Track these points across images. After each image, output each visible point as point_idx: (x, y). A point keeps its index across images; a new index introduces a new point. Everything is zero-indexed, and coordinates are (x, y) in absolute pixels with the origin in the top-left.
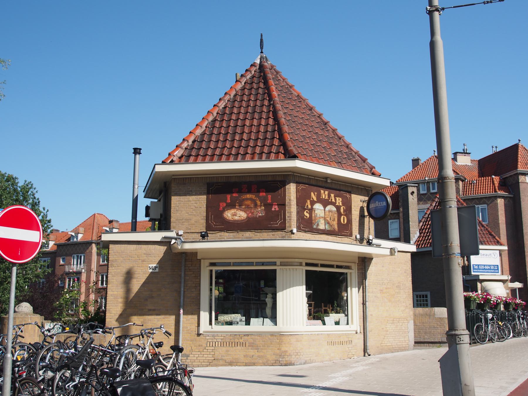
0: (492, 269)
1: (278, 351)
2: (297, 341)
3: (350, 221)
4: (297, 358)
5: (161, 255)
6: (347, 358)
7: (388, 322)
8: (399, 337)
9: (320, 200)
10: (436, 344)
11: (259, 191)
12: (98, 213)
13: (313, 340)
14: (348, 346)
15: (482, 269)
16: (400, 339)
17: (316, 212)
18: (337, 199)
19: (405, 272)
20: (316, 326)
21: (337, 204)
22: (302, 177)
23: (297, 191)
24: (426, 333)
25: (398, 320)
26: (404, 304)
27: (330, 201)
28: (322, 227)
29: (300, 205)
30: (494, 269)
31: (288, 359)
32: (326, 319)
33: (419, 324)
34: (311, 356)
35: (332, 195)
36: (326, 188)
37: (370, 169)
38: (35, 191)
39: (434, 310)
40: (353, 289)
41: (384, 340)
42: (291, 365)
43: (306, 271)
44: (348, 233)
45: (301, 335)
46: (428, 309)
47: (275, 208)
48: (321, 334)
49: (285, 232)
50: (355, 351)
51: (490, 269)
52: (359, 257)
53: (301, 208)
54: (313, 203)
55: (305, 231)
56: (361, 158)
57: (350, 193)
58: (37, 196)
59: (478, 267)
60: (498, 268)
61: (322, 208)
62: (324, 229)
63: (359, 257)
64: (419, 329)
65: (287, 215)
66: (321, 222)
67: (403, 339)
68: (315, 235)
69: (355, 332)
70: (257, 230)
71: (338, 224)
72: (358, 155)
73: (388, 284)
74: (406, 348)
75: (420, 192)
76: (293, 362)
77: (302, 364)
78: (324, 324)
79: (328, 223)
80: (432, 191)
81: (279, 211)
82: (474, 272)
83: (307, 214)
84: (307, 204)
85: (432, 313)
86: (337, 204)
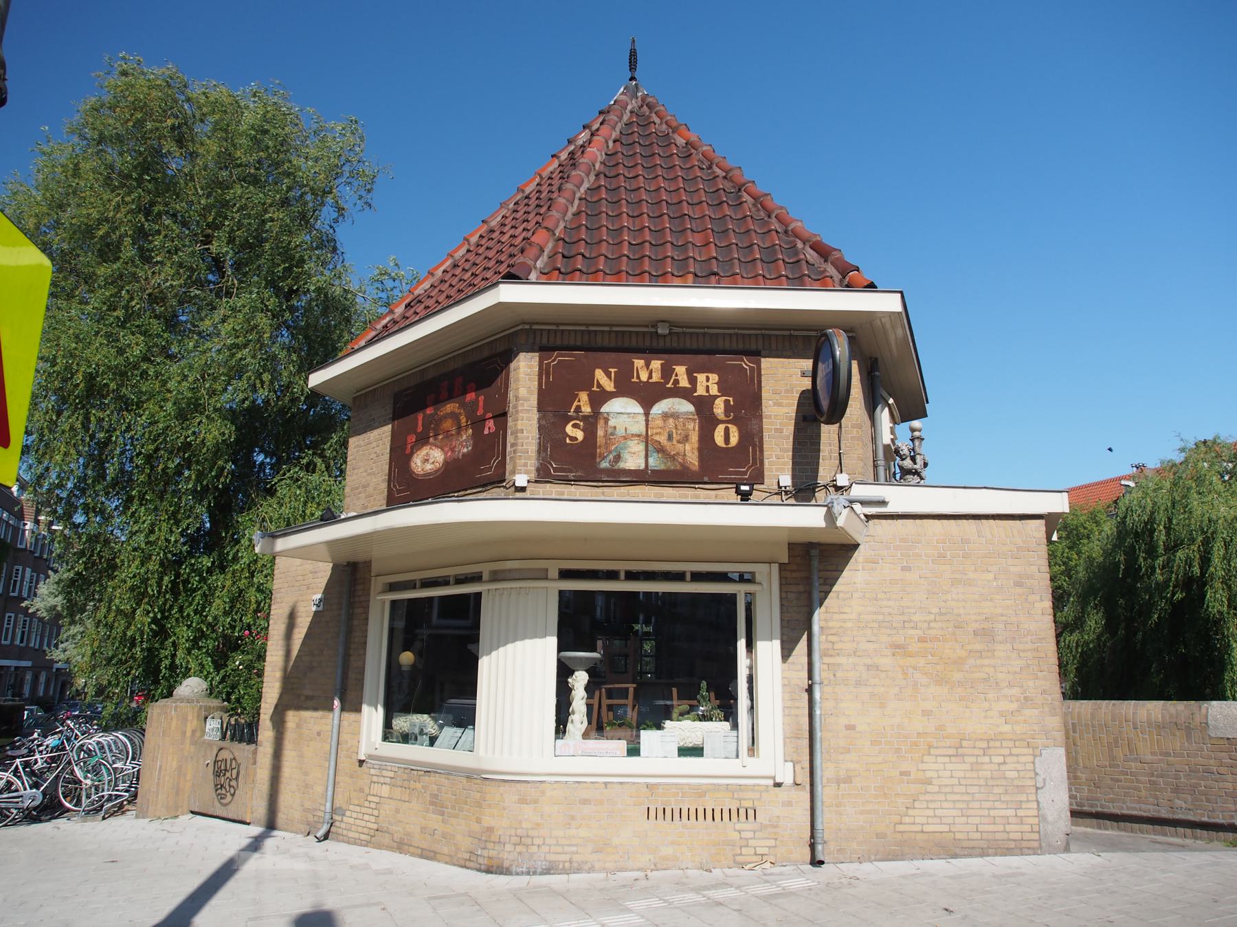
1: (476, 827)
2: (523, 801)
3: (752, 441)
4: (520, 853)
5: (329, 573)
6: (731, 863)
7: (933, 751)
8: (988, 804)
9: (626, 387)
10: (1221, 834)
11: (465, 393)
13: (585, 802)
14: (738, 826)
16: (992, 813)
17: (611, 423)
18: (701, 377)
19: (1018, 584)
21: (701, 391)
22: (563, 331)
23: (543, 371)
24: (1177, 790)
25: (984, 745)
26: (1015, 691)
27: (669, 385)
28: (633, 459)
29: (550, 409)
31: (493, 853)
32: (648, 737)
33: (1149, 758)
34: (574, 849)
35: (681, 370)
36: (649, 352)
37: (840, 277)
39: (1203, 711)
41: (911, 812)
42: (501, 873)
43: (561, 592)
44: (745, 473)
45: (538, 784)
46: (1186, 706)
48: (621, 783)
49: (504, 487)
50: (772, 843)
52: (791, 546)
53: (555, 416)
54: (600, 398)
55: (567, 481)
56: (817, 253)
57: (756, 354)
61: (640, 410)
62: (642, 467)
63: (791, 546)
64: (1153, 775)
65: (510, 439)
66: (629, 450)
67: (1011, 812)
68: (605, 489)
69: (771, 782)
70: (459, 491)
71: (700, 450)
72: (811, 247)
73: (932, 625)
74: (1024, 844)
76: (506, 864)
77: (535, 873)
78: (634, 751)
79: (661, 450)
81: (495, 435)
84: (576, 403)
85: (1198, 718)
86: (701, 391)
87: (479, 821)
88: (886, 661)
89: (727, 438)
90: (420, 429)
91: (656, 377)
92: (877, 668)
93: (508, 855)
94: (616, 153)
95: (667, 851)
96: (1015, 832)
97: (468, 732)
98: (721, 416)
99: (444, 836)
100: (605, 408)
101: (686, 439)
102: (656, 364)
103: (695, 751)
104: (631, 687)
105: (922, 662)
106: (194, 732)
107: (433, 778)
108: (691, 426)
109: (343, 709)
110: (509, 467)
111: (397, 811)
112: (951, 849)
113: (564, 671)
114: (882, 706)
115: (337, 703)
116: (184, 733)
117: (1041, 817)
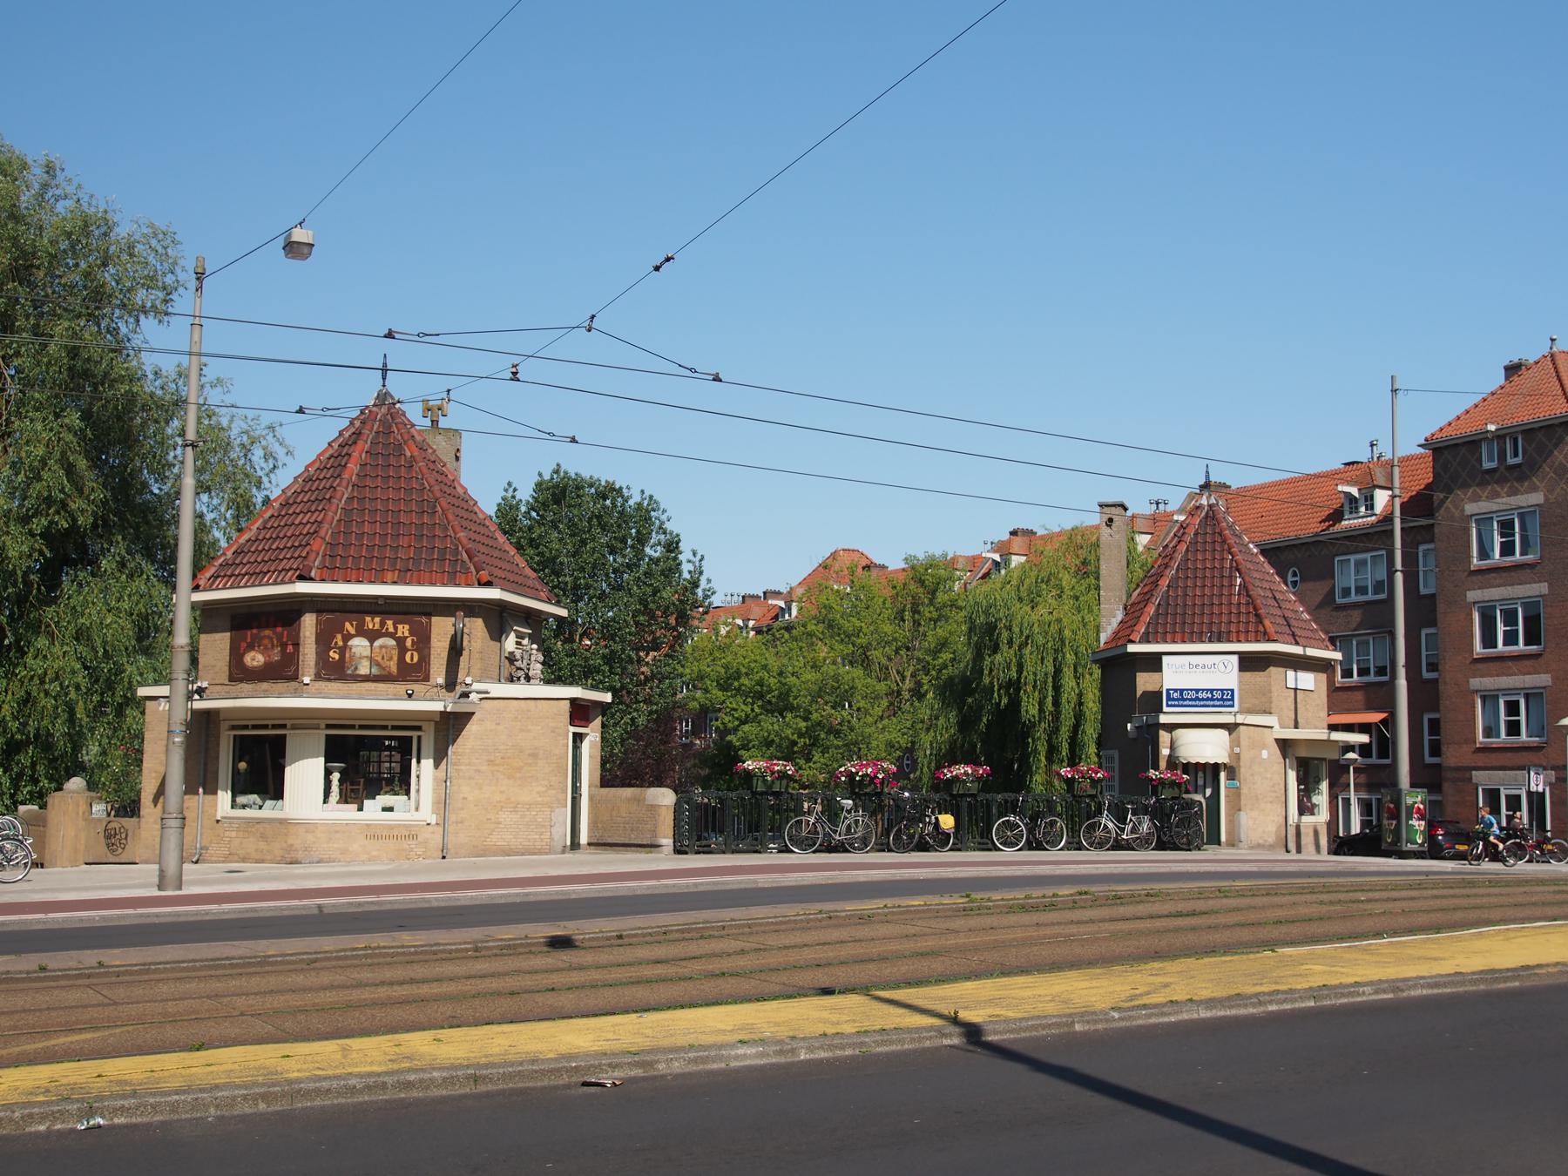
0: (1218, 700)
1: (284, 845)
3: (425, 660)
9: (361, 632)
11: (275, 626)
12: (846, 548)
13: (337, 832)
15: (1191, 700)
17: (353, 650)
18: (400, 627)
20: (349, 812)
21: (399, 634)
23: (318, 622)
26: (546, 783)
28: (364, 669)
30: (1222, 699)
35: (390, 623)
36: (373, 613)
38: (664, 518)
40: (423, 761)
47: (290, 649)
51: (1212, 699)
55: (329, 680)
57: (429, 615)
58: (668, 526)
59: (1181, 694)
60: (1233, 695)
61: (367, 643)
65: (301, 658)
75: (1481, 465)
78: (360, 809)
79: (378, 664)
80: (1511, 461)
81: (294, 653)
82: (1168, 706)
83: (334, 655)
86: (399, 634)
87: (286, 842)
88: (484, 768)
89: (412, 659)
90: (249, 640)
91: (377, 627)
92: (479, 771)
93: (300, 856)
94: (366, 464)
95: (375, 853)
96: (538, 845)
97: (280, 802)
98: (410, 647)
99: (268, 851)
100: (349, 643)
101: (391, 659)
102: (377, 620)
103: (390, 809)
104: (362, 780)
105: (501, 769)
106: (84, 813)
107: (262, 825)
108: (393, 652)
109: (204, 793)
110: (300, 672)
111: (241, 843)
112: (507, 852)
113: (328, 773)
114: (481, 789)
115: (201, 790)
116: (78, 813)
117: (552, 839)
